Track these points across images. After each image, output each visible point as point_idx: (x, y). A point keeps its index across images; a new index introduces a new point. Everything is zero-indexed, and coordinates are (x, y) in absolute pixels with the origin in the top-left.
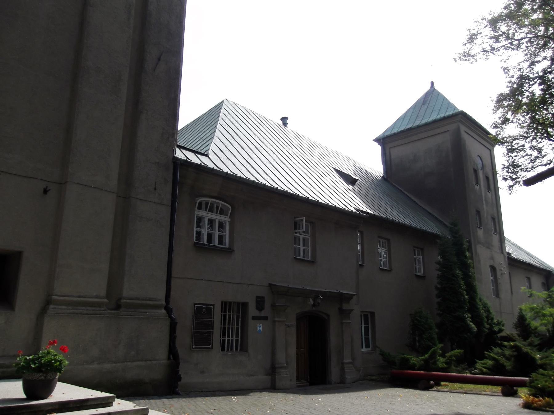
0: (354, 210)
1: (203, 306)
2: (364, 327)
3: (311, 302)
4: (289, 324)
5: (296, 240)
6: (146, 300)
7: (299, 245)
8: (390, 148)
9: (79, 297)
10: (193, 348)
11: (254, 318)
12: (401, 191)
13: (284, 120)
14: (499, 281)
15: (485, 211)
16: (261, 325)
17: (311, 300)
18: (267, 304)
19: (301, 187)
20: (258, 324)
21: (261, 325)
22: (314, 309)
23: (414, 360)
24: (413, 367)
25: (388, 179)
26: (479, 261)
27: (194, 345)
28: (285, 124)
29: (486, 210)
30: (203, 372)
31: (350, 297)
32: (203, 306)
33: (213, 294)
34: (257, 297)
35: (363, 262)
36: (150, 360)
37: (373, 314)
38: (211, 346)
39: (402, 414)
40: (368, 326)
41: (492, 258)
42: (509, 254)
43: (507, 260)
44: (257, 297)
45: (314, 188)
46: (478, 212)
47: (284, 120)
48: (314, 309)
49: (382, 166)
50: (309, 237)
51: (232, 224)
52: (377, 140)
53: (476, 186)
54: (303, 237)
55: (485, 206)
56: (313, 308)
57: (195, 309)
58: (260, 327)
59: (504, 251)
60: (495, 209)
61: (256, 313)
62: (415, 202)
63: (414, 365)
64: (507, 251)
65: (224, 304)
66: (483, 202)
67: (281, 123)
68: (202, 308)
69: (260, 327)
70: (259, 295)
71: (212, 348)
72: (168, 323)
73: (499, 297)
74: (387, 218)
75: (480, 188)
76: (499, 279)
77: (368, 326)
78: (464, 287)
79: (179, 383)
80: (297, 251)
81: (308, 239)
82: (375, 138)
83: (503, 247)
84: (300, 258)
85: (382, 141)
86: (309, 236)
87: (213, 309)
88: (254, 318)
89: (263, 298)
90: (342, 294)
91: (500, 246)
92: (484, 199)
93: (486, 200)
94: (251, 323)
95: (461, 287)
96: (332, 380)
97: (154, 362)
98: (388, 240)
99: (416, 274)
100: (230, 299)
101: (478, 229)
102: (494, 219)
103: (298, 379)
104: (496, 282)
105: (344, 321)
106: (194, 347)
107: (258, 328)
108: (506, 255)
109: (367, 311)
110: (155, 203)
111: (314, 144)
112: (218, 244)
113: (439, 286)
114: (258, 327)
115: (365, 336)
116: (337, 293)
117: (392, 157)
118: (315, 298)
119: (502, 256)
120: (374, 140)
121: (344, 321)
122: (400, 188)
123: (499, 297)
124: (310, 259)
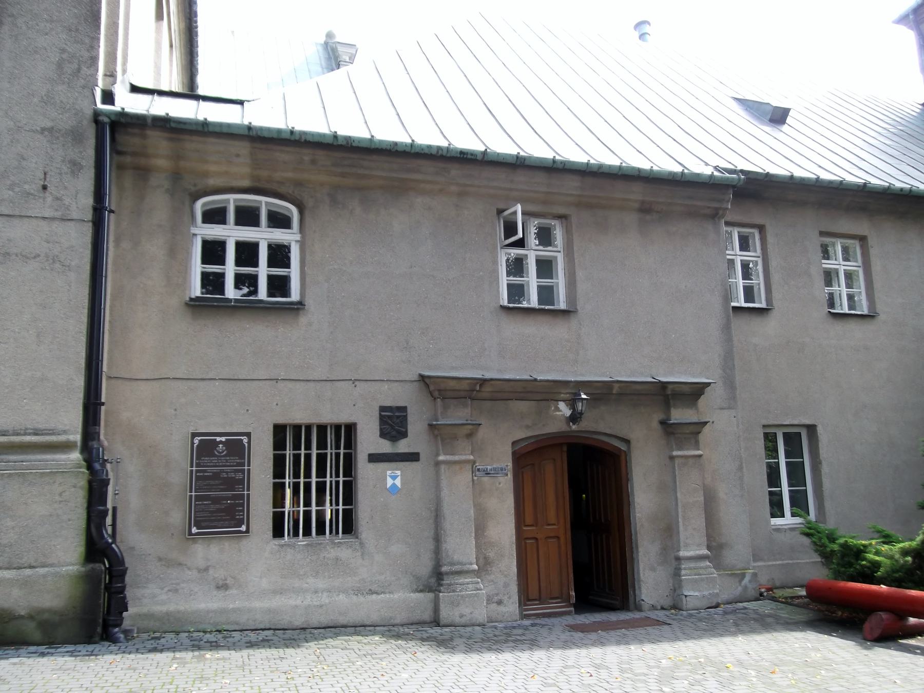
1: (218, 439)
2: (787, 464)
3: (565, 410)
4: (489, 467)
5: (829, 277)
6: (25, 434)
7: (839, 286)
9: (36, 433)
10: (190, 534)
11: (374, 458)
16: (399, 473)
17: (562, 405)
18: (416, 426)
19: (843, 158)
20: (389, 473)
21: (399, 473)
22: (574, 427)
23: (877, 553)
24: (868, 575)
27: (194, 526)
30: (223, 587)
31: (696, 392)
32: (218, 439)
33: (248, 410)
34: (383, 409)
35: (769, 300)
36: (31, 567)
37: (811, 429)
38: (244, 528)
39: (894, 692)
44: (383, 409)
45: (893, 157)
48: (574, 427)
50: (854, 266)
51: (302, 244)
52: (903, 20)
56: (571, 424)
57: (195, 445)
58: (394, 478)
61: (385, 447)
63: (876, 565)
65: (279, 431)
68: (215, 444)
69: (394, 478)
70: (388, 403)
71: (247, 531)
72: (82, 482)
74: (792, 177)
77: (778, 463)
79: (125, 614)
81: (858, 271)
84: (530, 306)
85: (911, 17)
86: (860, 267)
87: (246, 445)
88: (374, 458)
89: (404, 409)
90: (664, 385)
94: (365, 470)
96: (643, 600)
97: (42, 571)
98: (863, 239)
100: (300, 417)
103: (526, 597)
106: (194, 530)
107: (390, 482)
110: (44, 218)
112: (509, 303)
114: (388, 478)
115: (790, 485)
118: (572, 402)
121: (675, 453)
124: (866, 312)
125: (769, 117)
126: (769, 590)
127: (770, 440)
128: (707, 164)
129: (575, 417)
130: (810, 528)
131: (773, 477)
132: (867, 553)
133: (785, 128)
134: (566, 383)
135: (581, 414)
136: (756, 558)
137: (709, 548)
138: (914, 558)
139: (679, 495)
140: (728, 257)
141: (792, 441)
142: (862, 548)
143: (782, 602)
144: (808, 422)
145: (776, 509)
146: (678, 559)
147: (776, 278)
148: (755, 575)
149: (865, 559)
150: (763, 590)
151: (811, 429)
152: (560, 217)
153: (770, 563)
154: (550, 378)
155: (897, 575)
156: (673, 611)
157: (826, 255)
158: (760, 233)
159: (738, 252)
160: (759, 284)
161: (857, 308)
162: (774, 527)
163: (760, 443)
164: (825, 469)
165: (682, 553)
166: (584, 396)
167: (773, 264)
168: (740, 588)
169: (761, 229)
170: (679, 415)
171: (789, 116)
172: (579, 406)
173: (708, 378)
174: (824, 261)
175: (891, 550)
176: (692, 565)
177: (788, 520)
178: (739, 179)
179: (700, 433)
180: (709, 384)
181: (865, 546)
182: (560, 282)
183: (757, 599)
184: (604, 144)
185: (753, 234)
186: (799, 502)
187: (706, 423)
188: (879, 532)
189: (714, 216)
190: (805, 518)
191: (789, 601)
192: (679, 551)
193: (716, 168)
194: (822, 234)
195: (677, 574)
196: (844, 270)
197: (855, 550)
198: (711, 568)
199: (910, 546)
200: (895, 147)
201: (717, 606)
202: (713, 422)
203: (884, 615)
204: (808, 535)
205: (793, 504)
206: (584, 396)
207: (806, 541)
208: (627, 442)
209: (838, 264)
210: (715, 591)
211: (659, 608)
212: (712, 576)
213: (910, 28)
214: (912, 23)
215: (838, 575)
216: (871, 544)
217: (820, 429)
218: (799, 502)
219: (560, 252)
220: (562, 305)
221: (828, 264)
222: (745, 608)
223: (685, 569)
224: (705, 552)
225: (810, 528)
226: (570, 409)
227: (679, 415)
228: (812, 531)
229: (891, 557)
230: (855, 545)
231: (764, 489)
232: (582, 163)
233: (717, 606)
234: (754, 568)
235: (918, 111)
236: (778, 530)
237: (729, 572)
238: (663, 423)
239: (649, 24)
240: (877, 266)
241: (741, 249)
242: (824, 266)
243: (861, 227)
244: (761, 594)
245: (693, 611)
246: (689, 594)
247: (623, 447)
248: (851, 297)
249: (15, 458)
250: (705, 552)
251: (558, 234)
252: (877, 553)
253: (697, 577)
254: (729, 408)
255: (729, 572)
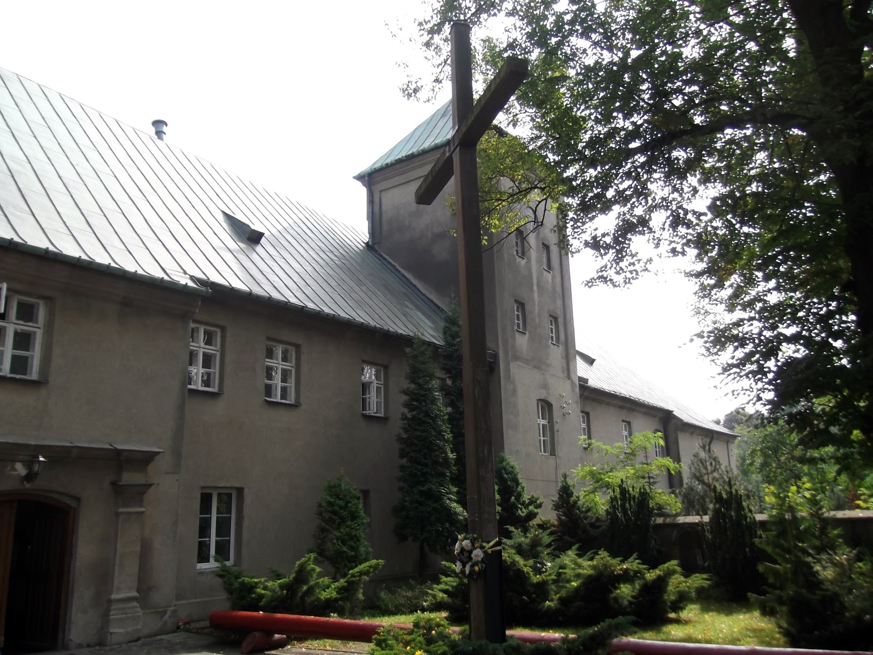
0: (191, 284)
3: (21, 469)
8: (381, 191)
12: (394, 267)
13: (158, 125)
14: (556, 427)
15: (536, 303)
22: (28, 486)
23: (265, 588)
25: (376, 247)
26: (514, 391)
28: (159, 134)
29: (537, 303)
31: (147, 458)
35: (220, 389)
37: (240, 491)
40: (209, 516)
41: (545, 386)
42: (583, 381)
43: (577, 390)
46: (521, 305)
47: (158, 125)
48: (28, 486)
49: (367, 222)
52: (360, 178)
53: (518, 260)
54: (204, 352)
55: (536, 295)
56: (25, 483)
59: (572, 375)
60: (559, 302)
62: (415, 286)
63: (261, 597)
64: (579, 375)
66: (532, 286)
67: (152, 130)
73: (555, 455)
75: (529, 261)
76: (557, 422)
78: (448, 436)
80: (268, 390)
81: (291, 371)
82: (356, 173)
83: (571, 368)
86: (293, 367)
90: (118, 452)
91: (565, 366)
92: (535, 281)
93: (538, 286)
95: (444, 436)
96: (71, 640)
98: (298, 347)
99: (364, 412)
101: (517, 335)
102: (555, 319)
104: (550, 430)
105: (120, 510)
108: (577, 383)
109: (220, 486)
111: (204, 173)
112: (281, 399)
113: (404, 436)
115: (217, 535)
116: (111, 449)
117: (384, 207)
118: (29, 463)
119: (568, 384)
120: (354, 178)
121: (120, 510)
122: (393, 263)
123: (555, 455)
125: (247, 236)
126: (186, 623)
127: (206, 500)
128: (185, 273)
129: (30, 477)
130: (223, 571)
131: (204, 529)
132: (257, 588)
133: (259, 249)
134: (26, 446)
135: (37, 474)
136: (179, 597)
137: (138, 590)
138: (288, 591)
139: (118, 546)
140: (191, 348)
141: (225, 500)
142: (254, 584)
143: (194, 633)
144: (237, 485)
145: (203, 557)
146: (110, 601)
147: (228, 369)
148: (175, 611)
149: (255, 593)
150: (180, 624)
151: (240, 491)
152: (47, 299)
153: (192, 601)
154: (10, 441)
155: (274, 604)
156: (97, 648)
157: (270, 354)
158: (222, 332)
159: (202, 345)
160: (215, 373)
161: (288, 398)
162: (198, 571)
163: (197, 504)
164: (246, 523)
165: (114, 596)
166: (42, 459)
167: (228, 358)
168: (160, 624)
169: (223, 329)
170: (129, 478)
171: (263, 237)
172: (36, 468)
173: (159, 448)
174: (267, 360)
175: (274, 584)
176: (121, 606)
177: (212, 565)
178: (208, 291)
179: (145, 492)
180: (158, 453)
181: (256, 583)
182: (36, 355)
183: (174, 632)
184: (119, 161)
185: (216, 332)
186: (222, 551)
187: (151, 485)
188: (274, 572)
189: (185, 317)
190: (221, 563)
191: (198, 632)
192: (111, 594)
193: (192, 278)
194: (268, 339)
195: (106, 615)
196: (282, 368)
197: (248, 586)
198: (137, 607)
199: (285, 581)
200: (334, 278)
201: (138, 640)
202: (158, 484)
203: (257, 634)
204: (220, 576)
205: (217, 551)
206: (42, 459)
207: (219, 581)
208: (78, 499)
209: (278, 364)
210: (138, 627)
211: (85, 645)
212: (137, 614)
213: (364, 185)
214: (366, 183)
215: (236, 607)
216: (260, 581)
217: (246, 491)
218: (222, 551)
219: (40, 328)
220: (34, 375)
221: (269, 362)
222: (162, 640)
223: (114, 610)
224: (135, 594)
225: (223, 571)
226: (26, 469)
227: (129, 478)
228: (224, 573)
229: (273, 591)
230: (249, 583)
231: (194, 539)
232: (74, 257)
233: (138, 640)
234: (175, 605)
235: (361, 248)
236: (202, 573)
237: (153, 610)
238: (114, 484)
239: (167, 125)
240: (304, 368)
241: (206, 344)
242: (267, 363)
243: (299, 339)
244: (178, 628)
245: (116, 646)
246: (115, 631)
247: (73, 504)
248: (284, 390)
249: (543, 634)
250: (135, 594)
251: (42, 314)
252: (265, 588)
253: (124, 616)
254: (173, 473)
255: (153, 610)
